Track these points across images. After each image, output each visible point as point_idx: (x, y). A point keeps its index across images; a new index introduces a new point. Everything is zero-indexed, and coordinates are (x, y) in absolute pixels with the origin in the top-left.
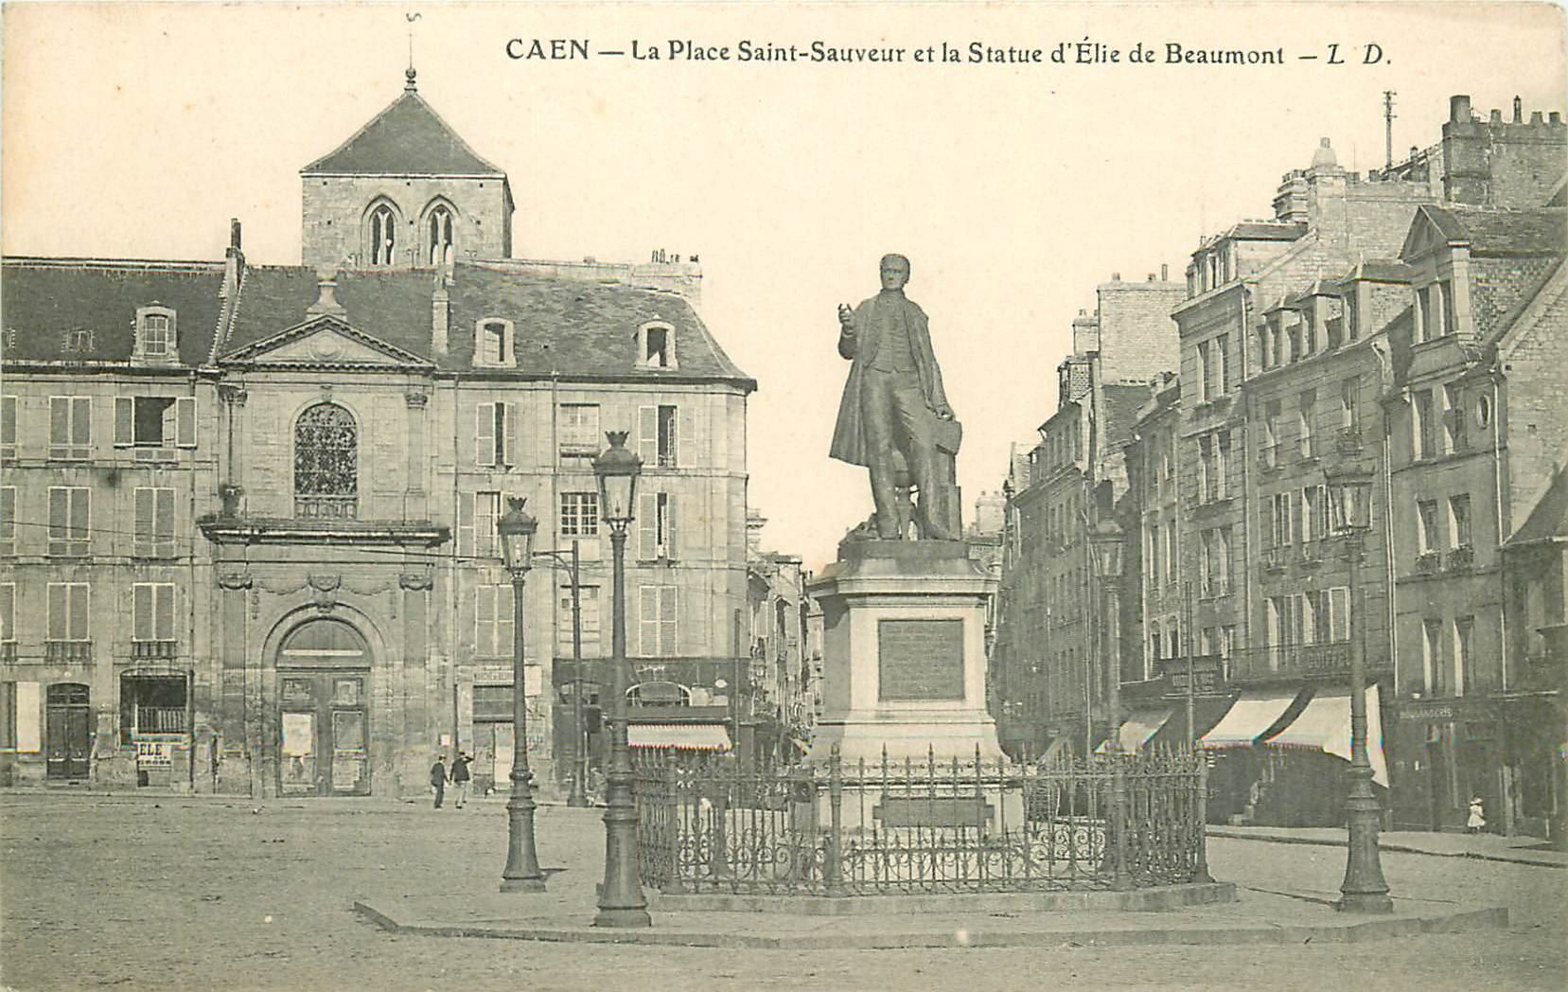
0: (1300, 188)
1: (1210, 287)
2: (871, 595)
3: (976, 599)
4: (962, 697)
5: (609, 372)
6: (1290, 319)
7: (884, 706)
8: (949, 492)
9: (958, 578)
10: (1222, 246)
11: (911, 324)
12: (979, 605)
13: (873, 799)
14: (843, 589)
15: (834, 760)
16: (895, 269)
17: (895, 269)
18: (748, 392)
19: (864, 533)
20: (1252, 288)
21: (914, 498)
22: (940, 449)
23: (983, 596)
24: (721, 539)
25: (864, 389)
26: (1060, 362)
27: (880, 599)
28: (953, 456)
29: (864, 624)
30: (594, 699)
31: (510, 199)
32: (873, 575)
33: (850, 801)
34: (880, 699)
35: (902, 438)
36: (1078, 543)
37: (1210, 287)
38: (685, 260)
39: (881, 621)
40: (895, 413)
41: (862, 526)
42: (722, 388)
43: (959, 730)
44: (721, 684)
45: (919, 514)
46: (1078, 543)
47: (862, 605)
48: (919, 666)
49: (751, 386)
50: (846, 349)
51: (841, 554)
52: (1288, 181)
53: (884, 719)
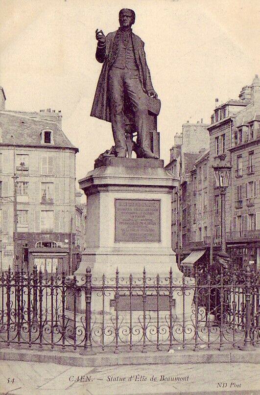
0: (248, 91)
1: (219, 119)
2: (111, 185)
3: (167, 190)
4: (160, 241)
5: (32, 144)
6: (245, 129)
7: (118, 245)
8: (154, 138)
9: (160, 177)
10: (224, 107)
11: (135, 46)
12: (169, 193)
13: (110, 295)
14: (96, 182)
15: (88, 277)
16: (127, 17)
17: (127, 17)
18: (76, 153)
19: (108, 155)
20: (233, 119)
21: (135, 139)
22: (150, 113)
23: (172, 188)
24: (67, 197)
25: (109, 78)
26: (171, 147)
27: (116, 188)
28: (155, 116)
29: (107, 200)
30: (26, 245)
31: (4, 96)
32: (114, 174)
33: (96, 298)
34: (116, 240)
35: (129, 108)
36: (175, 201)
37: (219, 119)
38: (57, 112)
39: (116, 200)
40: (125, 85)
41: (107, 152)
42: (67, 151)
43: (156, 260)
44: (67, 241)
45: (137, 147)
46: (175, 201)
47: (107, 191)
48: (136, 225)
49: (76, 150)
50: (100, 55)
51: (96, 166)
52: (244, 89)
53: (116, 253)
